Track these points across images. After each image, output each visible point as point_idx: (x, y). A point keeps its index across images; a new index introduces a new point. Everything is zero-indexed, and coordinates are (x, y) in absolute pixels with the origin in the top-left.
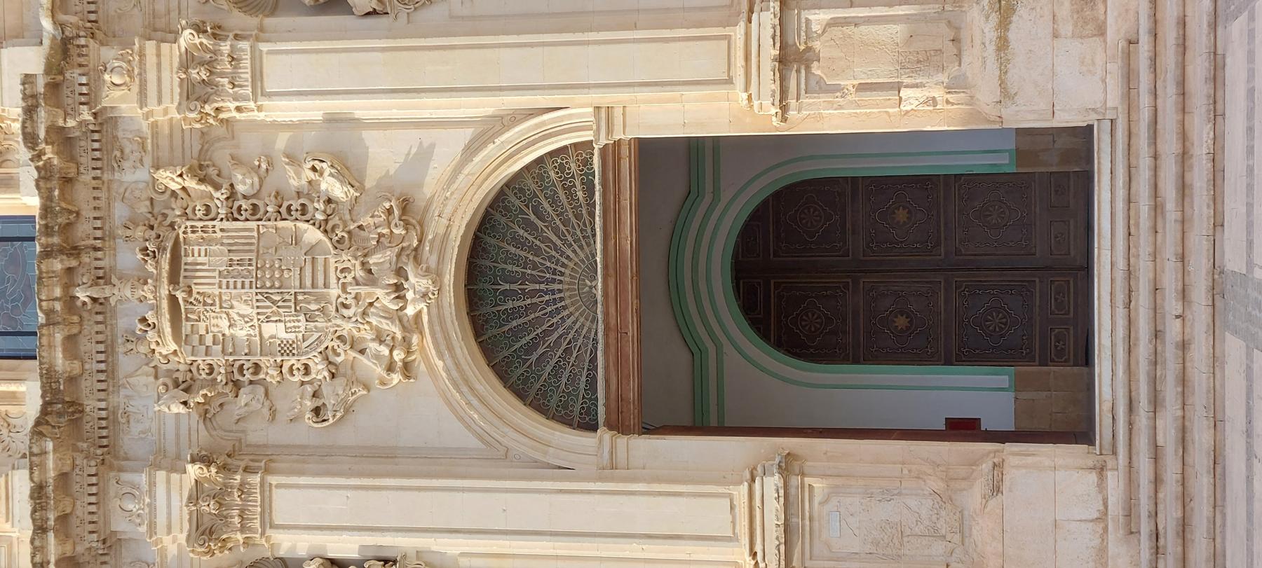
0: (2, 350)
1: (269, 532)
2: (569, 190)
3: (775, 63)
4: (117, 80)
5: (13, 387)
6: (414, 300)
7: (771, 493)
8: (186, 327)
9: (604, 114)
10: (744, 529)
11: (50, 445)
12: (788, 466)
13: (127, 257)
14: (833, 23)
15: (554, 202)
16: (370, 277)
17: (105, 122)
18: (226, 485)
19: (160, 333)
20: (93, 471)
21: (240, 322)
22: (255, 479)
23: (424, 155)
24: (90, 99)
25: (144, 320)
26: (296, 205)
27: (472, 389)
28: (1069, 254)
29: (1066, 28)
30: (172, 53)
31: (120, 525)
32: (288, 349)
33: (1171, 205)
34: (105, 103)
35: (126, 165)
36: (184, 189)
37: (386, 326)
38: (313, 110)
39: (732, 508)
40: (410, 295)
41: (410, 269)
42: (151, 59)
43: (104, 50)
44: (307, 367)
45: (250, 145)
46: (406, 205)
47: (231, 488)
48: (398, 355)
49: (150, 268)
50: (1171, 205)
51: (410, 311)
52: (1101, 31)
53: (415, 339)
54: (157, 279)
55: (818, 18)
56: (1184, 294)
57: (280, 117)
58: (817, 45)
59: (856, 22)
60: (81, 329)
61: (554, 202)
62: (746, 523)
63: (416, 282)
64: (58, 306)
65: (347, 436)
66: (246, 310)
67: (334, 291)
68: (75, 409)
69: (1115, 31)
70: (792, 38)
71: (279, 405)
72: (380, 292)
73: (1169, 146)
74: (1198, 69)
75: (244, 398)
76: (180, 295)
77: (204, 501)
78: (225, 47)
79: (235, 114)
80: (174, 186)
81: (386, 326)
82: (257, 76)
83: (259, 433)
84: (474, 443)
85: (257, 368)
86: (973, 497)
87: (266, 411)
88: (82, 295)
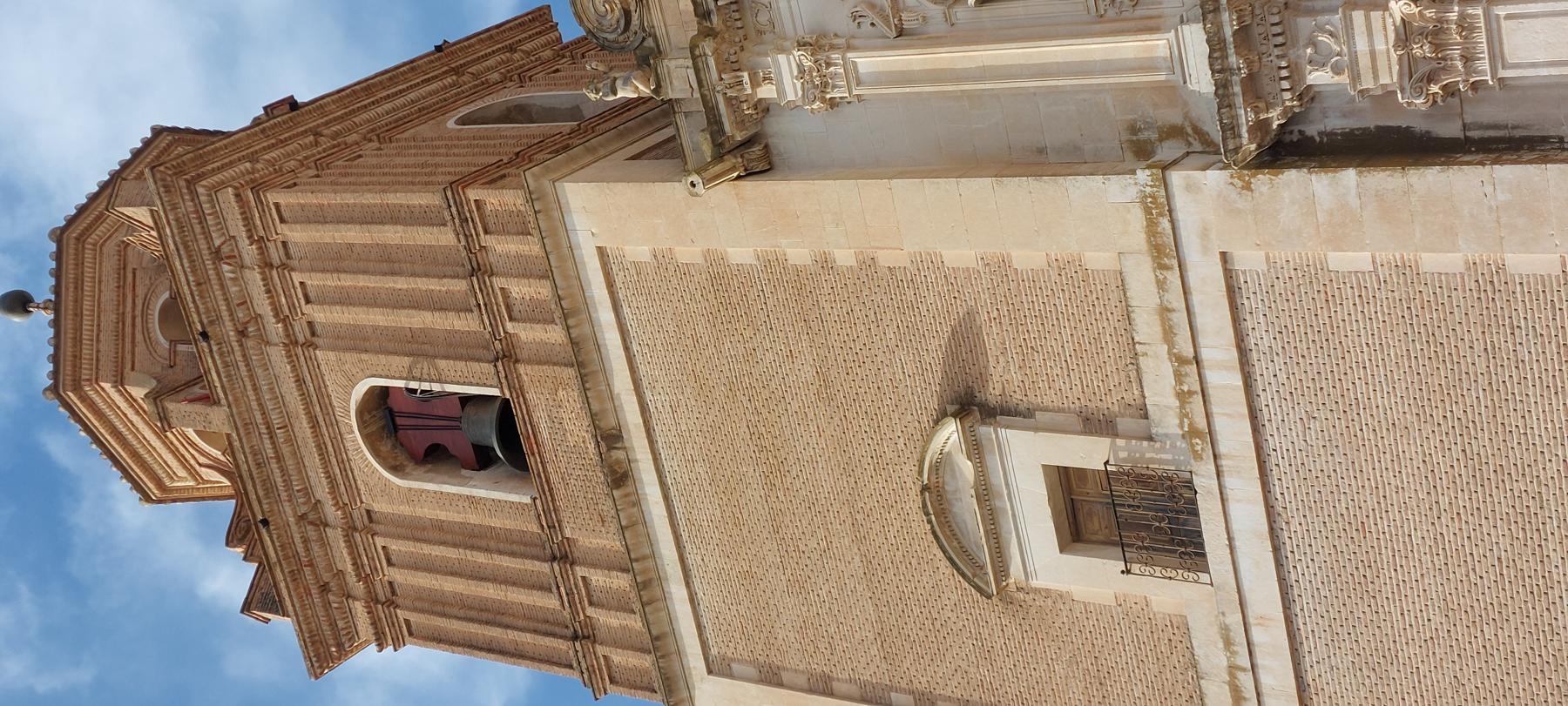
0: (777, 2)
3: (623, 470)
18: (1440, 20)
20: (1276, 19)
28: (252, 189)
47: (1448, 24)
60: (386, 403)
77: (1417, 43)
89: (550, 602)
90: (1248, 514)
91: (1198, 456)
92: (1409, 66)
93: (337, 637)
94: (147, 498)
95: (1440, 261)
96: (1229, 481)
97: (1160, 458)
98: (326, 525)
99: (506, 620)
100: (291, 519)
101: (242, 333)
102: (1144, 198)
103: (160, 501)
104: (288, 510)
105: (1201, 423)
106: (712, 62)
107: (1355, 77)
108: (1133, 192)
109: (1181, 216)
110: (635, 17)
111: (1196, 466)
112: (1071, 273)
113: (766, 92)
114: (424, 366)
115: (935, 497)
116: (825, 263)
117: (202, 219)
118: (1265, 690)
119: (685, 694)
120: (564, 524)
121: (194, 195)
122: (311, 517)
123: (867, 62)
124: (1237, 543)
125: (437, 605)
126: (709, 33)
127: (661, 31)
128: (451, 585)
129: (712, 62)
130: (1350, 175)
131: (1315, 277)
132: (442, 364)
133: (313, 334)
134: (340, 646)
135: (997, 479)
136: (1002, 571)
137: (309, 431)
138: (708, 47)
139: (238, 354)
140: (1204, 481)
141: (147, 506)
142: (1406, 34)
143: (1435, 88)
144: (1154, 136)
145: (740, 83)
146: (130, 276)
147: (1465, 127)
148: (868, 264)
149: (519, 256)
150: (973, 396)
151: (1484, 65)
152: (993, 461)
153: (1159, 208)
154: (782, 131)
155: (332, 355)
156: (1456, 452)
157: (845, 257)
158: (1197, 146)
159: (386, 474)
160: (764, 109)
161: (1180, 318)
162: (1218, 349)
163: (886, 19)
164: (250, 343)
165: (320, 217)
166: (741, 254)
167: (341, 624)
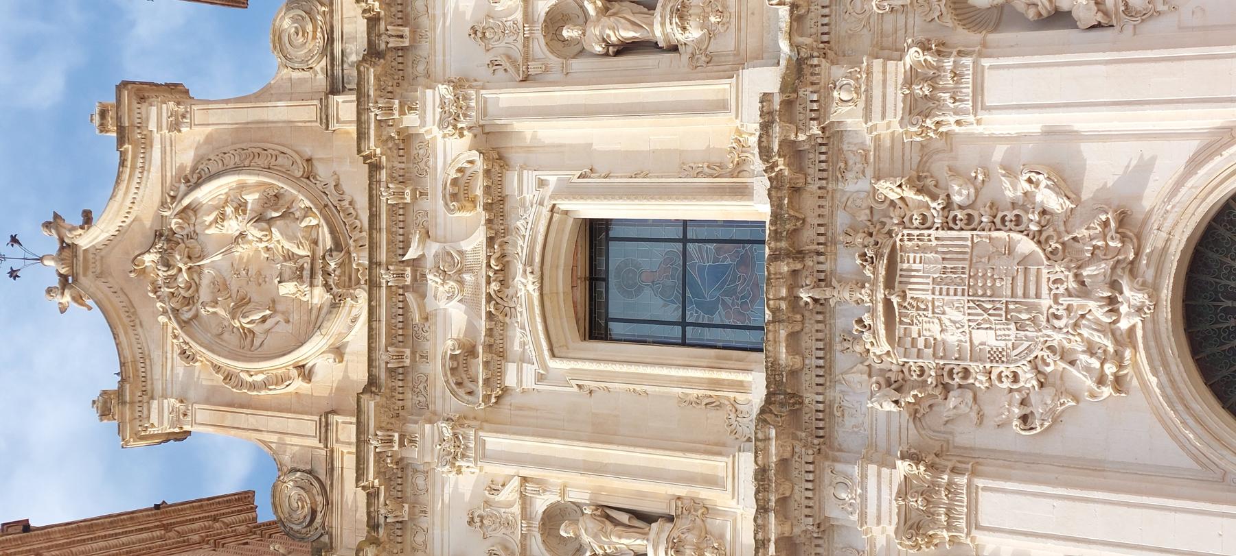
1: (974, 533)
4: (845, 96)
5: (740, 377)
6: (1128, 314)
8: (899, 330)
11: (773, 433)
16: (1083, 291)
17: (832, 136)
19: (875, 334)
21: (951, 328)
22: (962, 480)
23: (1144, 168)
24: (819, 115)
25: (860, 321)
26: (1010, 216)
27: (1187, 407)
30: (899, 71)
31: (833, 512)
32: (997, 356)
35: (849, 175)
36: (902, 198)
37: (1097, 338)
38: (1032, 123)
40: (1124, 309)
43: (834, 68)
44: (1015, 375)
45: (967, 157)
48: (1110, 369)
49: (868, 273)
51: (1124, 325)
53: (1128, 354)
54: (874, 284)
63: (1131, 296)
64: (783, 305)
65: (1054, 446)
66: (957, 316)
67: (1046, 302)
71: (988, 410)
72: (1092, 305)
75: (952, 401)
76: (895, 300)
78: (949, 64)
79: (957, 129)
80: (893, 196)
81: (1097, 338)
82: (978, 90)
83: (966, 435)
85: (966, 373)
88: (805, 296)
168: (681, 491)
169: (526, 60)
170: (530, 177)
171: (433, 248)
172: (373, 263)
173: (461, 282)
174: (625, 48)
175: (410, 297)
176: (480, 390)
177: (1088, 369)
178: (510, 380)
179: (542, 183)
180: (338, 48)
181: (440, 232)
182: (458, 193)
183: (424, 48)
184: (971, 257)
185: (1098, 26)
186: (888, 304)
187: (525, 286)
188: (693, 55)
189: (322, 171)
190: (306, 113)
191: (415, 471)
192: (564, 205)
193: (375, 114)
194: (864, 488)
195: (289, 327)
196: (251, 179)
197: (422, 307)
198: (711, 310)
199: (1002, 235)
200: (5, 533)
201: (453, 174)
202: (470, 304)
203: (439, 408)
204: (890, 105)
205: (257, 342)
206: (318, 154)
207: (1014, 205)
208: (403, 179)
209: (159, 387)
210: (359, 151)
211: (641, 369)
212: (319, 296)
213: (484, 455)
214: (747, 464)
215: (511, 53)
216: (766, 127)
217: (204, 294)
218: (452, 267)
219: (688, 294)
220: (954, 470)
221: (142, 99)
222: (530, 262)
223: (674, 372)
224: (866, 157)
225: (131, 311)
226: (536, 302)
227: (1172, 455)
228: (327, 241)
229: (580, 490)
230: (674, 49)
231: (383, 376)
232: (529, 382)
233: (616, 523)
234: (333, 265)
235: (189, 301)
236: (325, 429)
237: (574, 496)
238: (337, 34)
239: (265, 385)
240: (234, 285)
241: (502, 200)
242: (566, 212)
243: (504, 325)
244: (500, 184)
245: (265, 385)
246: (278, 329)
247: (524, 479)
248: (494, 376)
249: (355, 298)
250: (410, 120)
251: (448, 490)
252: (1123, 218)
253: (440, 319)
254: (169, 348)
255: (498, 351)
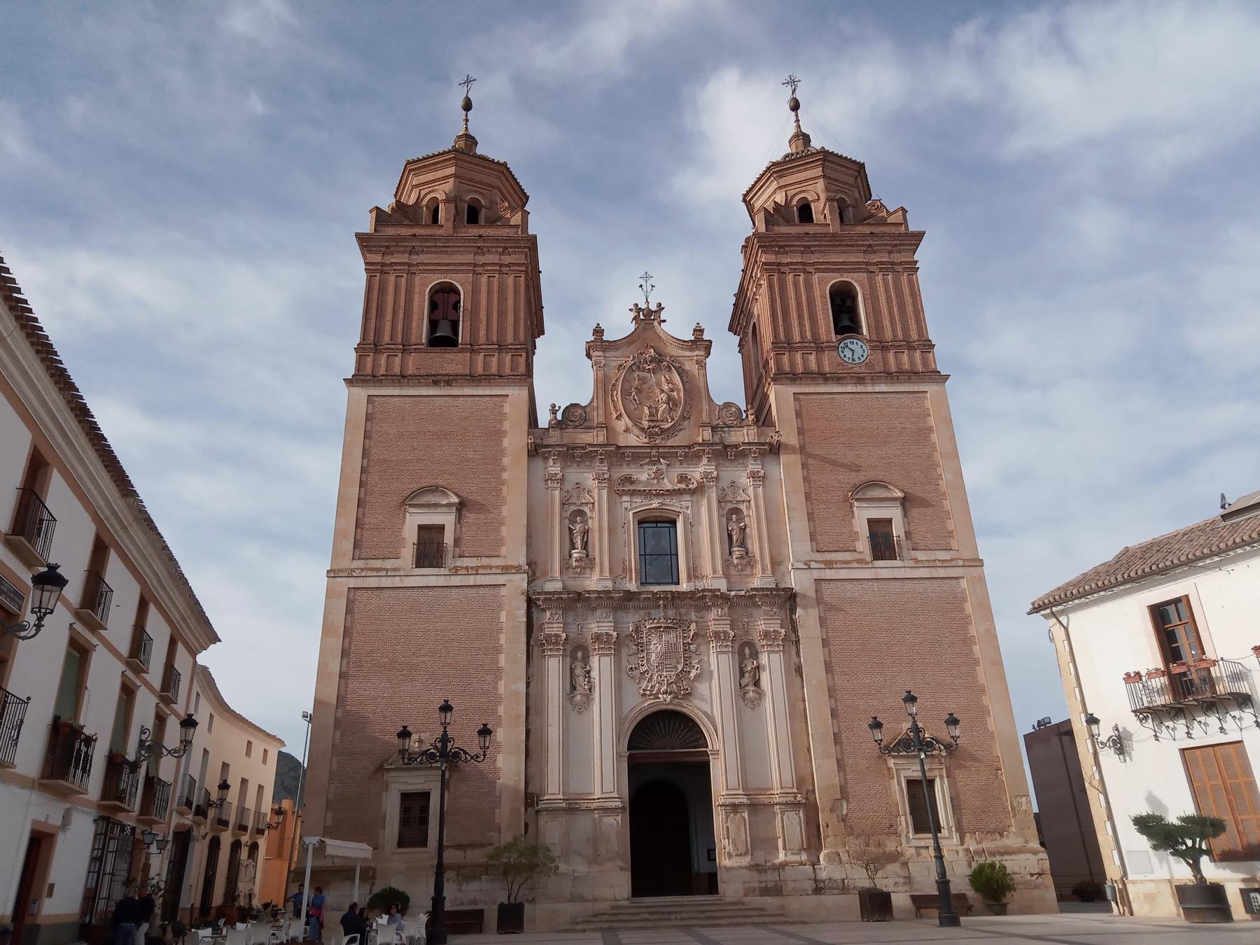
1: (598, 656)
2: (695, 741)
4: (719, 612)
5: (634, 580)
6: (663, 697)
7: (617, 804)
8: (653, 631)
9: (716, 753)
10: (203, 640)
11: (622, 595)
12: (623, 808)
13: (671, 613)
14: (745, 819)
15: (691, 736)
16: (669, 685)
17: (708, 608)
19: (651, 624)
21: (655, 647)
22: (613, 652)
23: (703, 700)
24: (714, 605)
25: (655, 619)
26: (688, 662)
27: (640, 714)
29: (746, 885)
30: (727, 628)
31: (598, 612)
32: (648, 660)
33: (703, 915)
34: (713, 609)
35: (696, 613)
36: (690, 630)
37: (656, 689)
38: (714, 667)
39: (611, 792)
40: (665, 696)
41: (671, 696)
42: (725, 622)
43: (727, 608)
44: (643, 665)
45: (703, 648)
46: (689, 694)
48: (648, 693)
49: (669, 621)
50: (703, 915)
51: (660, 696)
52: (746, 895)
53: (652, 697)
54: (666, 623)
55: (746, 815)
56: (682, 919)
57: (711, 657)
58: (739, 815)
59: (745, 826)
61: (691, 736)
62: (608, 796)
63: (669, 698)
64: (658, 596)
65: (624, 676)
66: (659, 648)
67: (665, 674)
68: (630, 600)
69: (745, 899)
70: (741, 807)
71: (632, 657)
72: (665, 687)
73: (719, 914)
74: (742, 920)
75: (635, 647)
76: (662, 629)
78: (729, 644)
79: (712, 645)
80: (691, 627)
81: (656, 689)
82: (723, 653)
83: (624, 652)
84: (624, 714)
85: (642, 651)
86: (619, 863)
87: (630, 654)
88: (661, 602)
89: (387, 339)
90: (432, 581)
91: (450, 570)
92: (550, 636)
93: (369, 246)
94: (409, 163)
95: (503, 639)
96: (443, 577)
97: (450, 562)
98: (410, 255)
99: (379, 316)
100: (414, 244)
101: (479, 247)
102: (521, 566)
103: (406, 167)
104: (418, 244)
105: (459, 573)
106: (561, 449)
107: (548, 623)
108: (521, 563)
109: (516, 575)
110: (571, 423)
111: (447, 570)
112: (500, 542)
113: (551, 462)
114: (468, 316)
115: (434, 489)
116: (503, 469)
117: (517, 247)
118: (381, 578)
119: (360, 385)
120: (416, 354)
121: (527, 247)
122: (414, 251)
123: (557, 493)
124: (425, 577)
125: (382, 291)
126: (568, 450)
127: (567, 430)
128: (390, 298)
129: (561, 449)
130: (525, 620)
131: (500, 608)
132: (469, 323)
133: (477, 274)
134: (366, 246)
135: (440, 510)
136: (411, 506)
137: (445, 262)
138: (565, 449)
139: (472, 244)
140: (442, 571)
141: (405, 162)
142: (557, 636)
143: (544, 641)
144: (533, 568)
145: (554, 456)
146: (490, 189)
147: (533, 646)
148: (503, 483)
149: (505, 364)
150: (464, 507)
151: (549, 653)
152: (445, 510)
153: (518, 569)
154: (539, 463)
155: (471, 280)
156: (452, 637)
157: (505, 476)
158: (530, 579)
159: (430, 287)
160: (546, 459)
161: (489, 571)
162: (480, 580)
163: (567, 500)
164: (475, 249)
165: (516, 287)
166: (506, 442)
167: (374, 249)
168: (597, 560)
169: (725, 502)
170: (689, 504)
171: (664, 467)
172: (659, 447)
173: (654, 478)
174: (730, 536)
175: (648, 460)
176: (621, 488)
177: (647, 686)
178: (625, 498)
179: (687, 508)
180: (726, 429)
181: (669, 470)
182: (683, 478)
183: (727, 464)
184: (676, 651)
185: (741, 685)
186: (661, 627)
187: (655, 503)
188: (729, 560)
189: (686, 423)
190: (705, 418)
191: (591, 461)
192: (681, 517)
193: (707, 449)
194: (607, 622)
195: (633, 409)
196: (682, 394)
197: (645, 464)
198: (651, 564)
199: (683, 661)
200: (552, 624)
201: (689, 477)
202: (647, 483)
203: (612, 470)
204: (718, 626)
205: (627, 397)
206: (692, 422)
207: (690, 663)
208: (686, 455)
209: (607, 354)
210: (695, 444)
211: (632, 545)
212: (646, 424)
213: (600, 489)
214: (609, 585)
215: (727, 497)
216: (710, 590)
217: (642, 374)
218: (659, 475)
219: (654, 557)
220: (615, 649)
221: (706, 348)
222: (662, 504)
223: (633, 557)
224: (701, 618)
225: (633, 342)
226: (650, 507)
227: (626, 709)
228: (667, 426)
229: (593, 524)
230: (730, 554)
231: (622, 451)
232: (625, 505)
233: (584, 536)
234: (656, 430)
235: (638, 368)
236: (600, 426)
237: (590, 521)
238: (731, 429)
239: (613, 401)
240: (645, 386)
241: (682, 494)
242: (679, 516)
243: (642, 495)
244: (685, 494)
245: (613, 401)
246: (632, 405)
247: (593, 503)
248: (624, 493)
249: (645, 438)
250: (705, 461)
251: (586, 475)
252: (689, 694)
253: (641, 470)
254: (622, 359)
255: (633, 493)
